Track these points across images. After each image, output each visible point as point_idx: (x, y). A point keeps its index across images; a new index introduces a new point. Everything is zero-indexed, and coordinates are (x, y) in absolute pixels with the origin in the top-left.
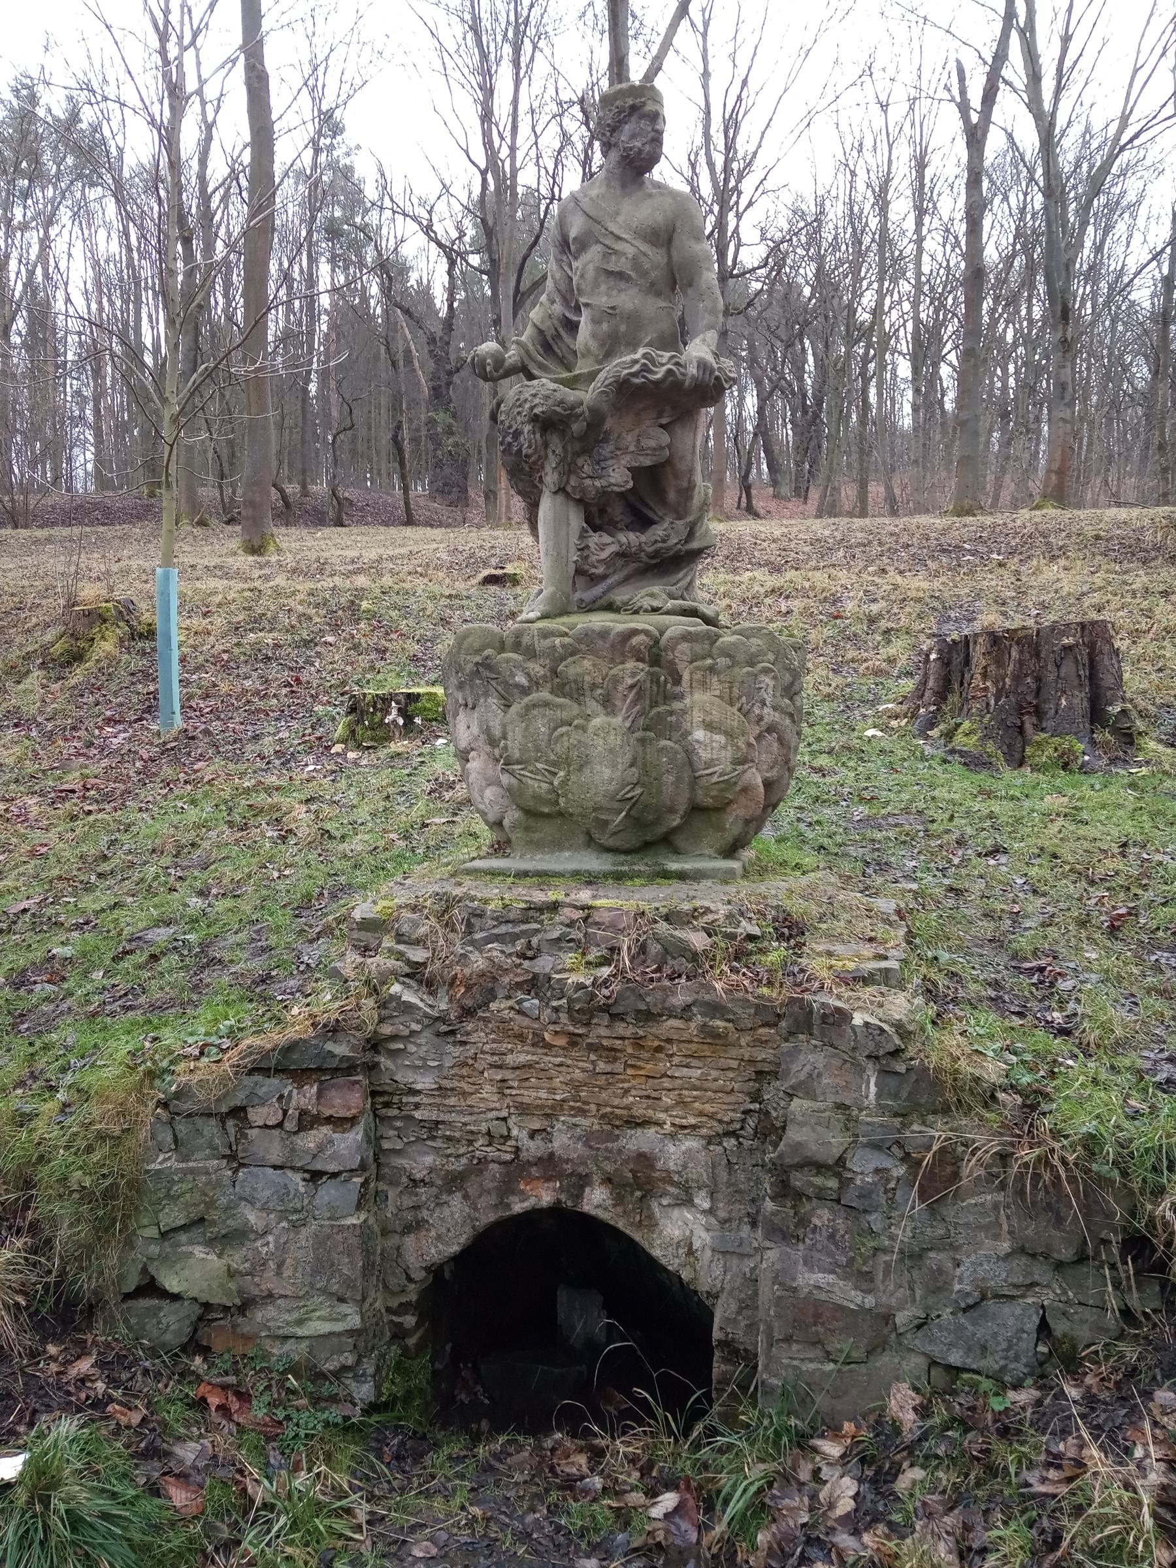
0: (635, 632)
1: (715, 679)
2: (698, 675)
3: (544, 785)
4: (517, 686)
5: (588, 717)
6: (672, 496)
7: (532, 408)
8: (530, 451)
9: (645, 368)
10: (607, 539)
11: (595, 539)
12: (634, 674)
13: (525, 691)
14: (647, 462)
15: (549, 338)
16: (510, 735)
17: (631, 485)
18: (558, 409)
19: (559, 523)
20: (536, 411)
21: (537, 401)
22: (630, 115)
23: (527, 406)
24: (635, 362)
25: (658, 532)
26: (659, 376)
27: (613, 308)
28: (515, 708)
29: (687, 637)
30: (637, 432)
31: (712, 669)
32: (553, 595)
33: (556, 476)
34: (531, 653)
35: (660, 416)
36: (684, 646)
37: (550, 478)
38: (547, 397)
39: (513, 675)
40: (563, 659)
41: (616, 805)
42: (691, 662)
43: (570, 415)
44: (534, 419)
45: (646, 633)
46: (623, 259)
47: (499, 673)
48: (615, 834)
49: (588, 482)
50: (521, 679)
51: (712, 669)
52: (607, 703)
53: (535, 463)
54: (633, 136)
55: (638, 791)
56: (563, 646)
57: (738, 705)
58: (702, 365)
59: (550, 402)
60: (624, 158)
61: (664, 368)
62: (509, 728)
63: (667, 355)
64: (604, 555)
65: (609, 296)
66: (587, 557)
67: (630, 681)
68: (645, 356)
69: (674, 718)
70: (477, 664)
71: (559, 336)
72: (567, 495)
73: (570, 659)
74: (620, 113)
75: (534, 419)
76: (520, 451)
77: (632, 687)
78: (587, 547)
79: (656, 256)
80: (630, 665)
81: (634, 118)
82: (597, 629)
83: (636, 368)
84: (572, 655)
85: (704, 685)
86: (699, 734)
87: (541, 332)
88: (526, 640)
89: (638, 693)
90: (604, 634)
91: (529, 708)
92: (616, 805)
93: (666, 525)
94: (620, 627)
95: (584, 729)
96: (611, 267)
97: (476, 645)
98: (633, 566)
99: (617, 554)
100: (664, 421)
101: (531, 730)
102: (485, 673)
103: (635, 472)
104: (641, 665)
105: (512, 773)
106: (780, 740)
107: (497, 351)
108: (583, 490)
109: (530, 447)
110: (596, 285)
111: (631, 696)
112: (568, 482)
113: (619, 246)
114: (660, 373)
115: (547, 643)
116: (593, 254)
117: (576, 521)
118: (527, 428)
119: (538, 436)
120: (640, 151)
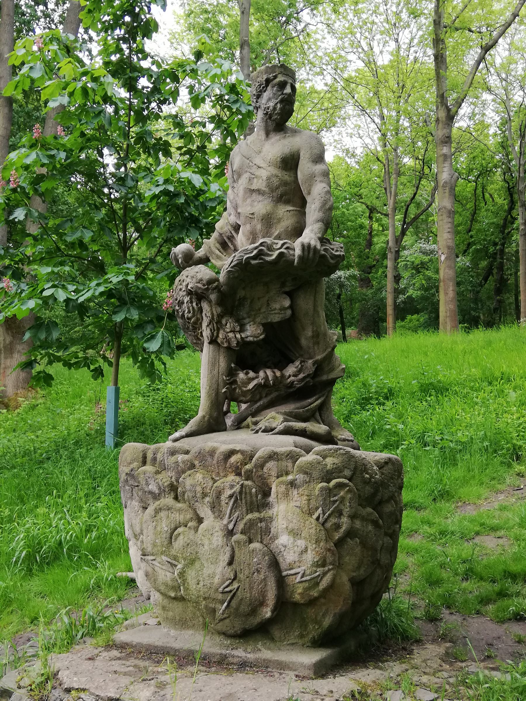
0: (232, 453)
1: (295, 492)
2: (283, 488)
3: (169, 574)
4: (150, 492)
5: (200, 520)
6: (304, 342)
7: (187, 286)
8: (190, 315)
9: (260, 254)
10: (251, 374)
11: (241, 375)
12: (232, 487)
13: (156, 497)
14: (276, 318)
15: (225, 238)
16: (145, 532)
17: (262, 337)
18: (199, 285)
19: (213, 363)
20: (189, 288)
21: (188, 280)
22: (267, 85)
23: (184, 284)
24: (256, 248)
25: (290, 370)
26: (274, 257)
27: (253, 214)
28: (150, 510)
29: (273, 456)
30: (266, 298)
31: (292, 484)
32: (204, 417)
33: (209, 331)
34: (163, 468)
35: (283, 285)
36: (271, 464)
37: (206, 333)
38: (192, 277)
39: (148, 484)
40: (184, 472)
41: (220, 597)
42: (278, 477)
43: (207, 289)
44: (190, 293)
45: (242, 452)
46: (261, 181)
47: (139, 482)
48: (221, 620)
49: (231, 335)
50: (153, 487)
51: (292, 484)
52: (215, 506)
53: (195, 323)
54: (269, 99)
55: (235, 585)
56: (183, 462)
57: (315, 516)
58: (307, 248)
59: (194, 280)
60: (266, 114)
61: (277, 252)
62: (144, 526)
63: (281, 242)
64: (251, 386)
65: (252, 205)
66: (235, 389)
67: (229, 492)
68: (261, 244)
69: (263, 524)
70: (127, 474)
71: (233, 237)
72: (219, 345)
73: (189, 472)
74: (260, 85)
75: (190, 293)
76: (183, 315)
77: (231, 497)
78: (235, 382)
79: (287, 177)
80: (231, 478)
81: (269, 88)
82: (207, 449)
83: (255, 252)
84: (189, 469)
85: (286, 495)
86: (284, 539)
87: (221, 235)
88: (159, 456)
89: (236, 501)
90: (212, 453)
91: (157, 511)
92: (220, 597)
93: (297, 363)
94: (224, 448)
95: (196, 529)
96: (254, 187)
97: (129, 460)
98: (274, 395)
99: (258, 386)
100: (287, 289)
101: (159, 529)
102: (131, 482)
103: (268, 327)
104: (238, 479)
105: (147, 562)
106: (363, 544)
107: (189, 250)
108: (229, 341)
109: (189, 312)
110: (245, 199)
111: (231, 503)
112: (218, 336)
113: (259, 172)
114: (276, 254)
115: (173, 459)
116: (243, 182)
117: (223, 363)
118: (187, 299)
119: (194, 304)
120: (275, 108)
